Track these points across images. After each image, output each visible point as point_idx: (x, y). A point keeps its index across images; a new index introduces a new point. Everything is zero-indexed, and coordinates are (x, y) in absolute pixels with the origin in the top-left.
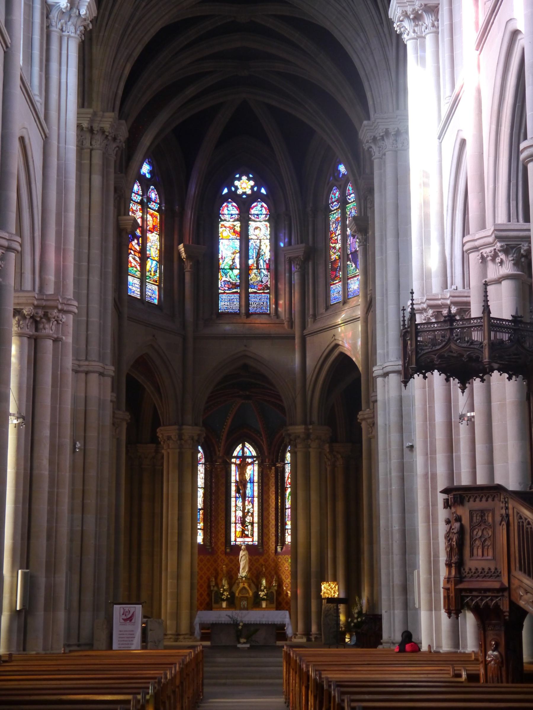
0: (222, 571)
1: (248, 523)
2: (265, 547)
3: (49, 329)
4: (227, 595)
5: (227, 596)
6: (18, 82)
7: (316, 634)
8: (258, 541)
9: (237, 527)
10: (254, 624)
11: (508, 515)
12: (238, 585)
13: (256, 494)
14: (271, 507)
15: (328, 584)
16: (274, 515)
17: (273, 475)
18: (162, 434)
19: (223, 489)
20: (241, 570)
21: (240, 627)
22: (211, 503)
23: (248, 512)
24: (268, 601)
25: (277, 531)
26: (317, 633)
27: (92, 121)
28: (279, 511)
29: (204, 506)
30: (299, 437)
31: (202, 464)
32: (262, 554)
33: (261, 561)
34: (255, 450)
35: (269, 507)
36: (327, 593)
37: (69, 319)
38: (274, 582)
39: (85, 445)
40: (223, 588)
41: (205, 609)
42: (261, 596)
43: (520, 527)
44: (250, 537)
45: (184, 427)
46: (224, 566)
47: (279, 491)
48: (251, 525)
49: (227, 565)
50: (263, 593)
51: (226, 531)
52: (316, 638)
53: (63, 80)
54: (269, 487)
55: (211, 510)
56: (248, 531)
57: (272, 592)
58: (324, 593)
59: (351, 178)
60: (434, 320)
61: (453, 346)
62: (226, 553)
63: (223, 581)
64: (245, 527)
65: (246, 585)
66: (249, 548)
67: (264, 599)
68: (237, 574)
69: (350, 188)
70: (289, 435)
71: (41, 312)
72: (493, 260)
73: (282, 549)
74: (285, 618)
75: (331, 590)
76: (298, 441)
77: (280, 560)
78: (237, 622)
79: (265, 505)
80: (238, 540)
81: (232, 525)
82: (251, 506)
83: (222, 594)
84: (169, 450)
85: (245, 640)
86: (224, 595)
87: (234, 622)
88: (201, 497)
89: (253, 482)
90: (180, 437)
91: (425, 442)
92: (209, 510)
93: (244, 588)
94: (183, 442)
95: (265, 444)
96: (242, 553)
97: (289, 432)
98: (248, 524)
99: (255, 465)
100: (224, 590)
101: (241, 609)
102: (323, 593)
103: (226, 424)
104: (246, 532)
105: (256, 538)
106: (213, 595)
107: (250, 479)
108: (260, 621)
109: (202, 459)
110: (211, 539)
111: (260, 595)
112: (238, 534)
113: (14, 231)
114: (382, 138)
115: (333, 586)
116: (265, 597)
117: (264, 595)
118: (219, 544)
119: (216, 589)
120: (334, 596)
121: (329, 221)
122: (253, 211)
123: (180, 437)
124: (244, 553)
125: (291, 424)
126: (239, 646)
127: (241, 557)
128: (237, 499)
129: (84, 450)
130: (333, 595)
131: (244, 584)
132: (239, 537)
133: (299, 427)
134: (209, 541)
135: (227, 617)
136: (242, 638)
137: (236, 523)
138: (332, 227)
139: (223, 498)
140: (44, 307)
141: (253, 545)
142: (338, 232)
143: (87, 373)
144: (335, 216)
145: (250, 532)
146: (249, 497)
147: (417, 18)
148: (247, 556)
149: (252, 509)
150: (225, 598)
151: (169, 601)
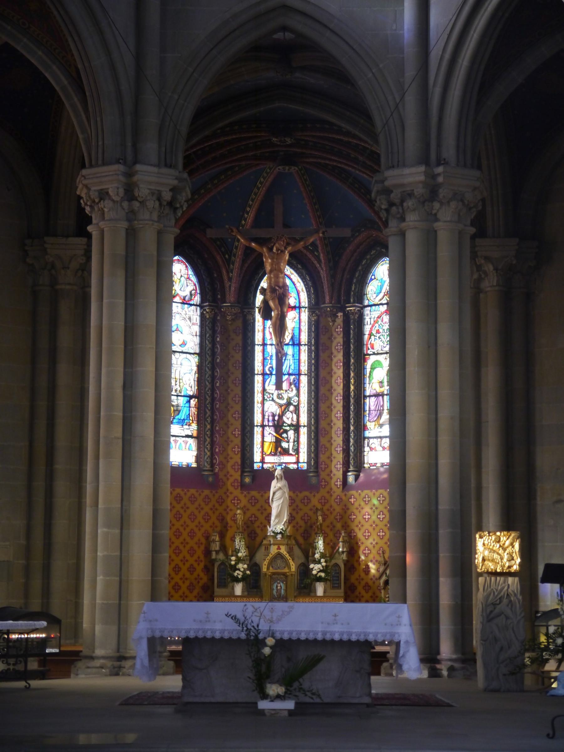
0: (235, 521)
1: (289, 426)
2: (323, 475)
5: (244, 572)
7: (451, 660)
8: (308, 463)
9: (266, 433)
10: (307, 641)
12: (267, 548)
13: (304, 368)
14: (335, 394)
15: (493, 538)
16: (341, 409)
17: (340, 330)
18: (86, 186)
19: (238, 357)
20: (273, 518)
21: (267, 651)
22: (213, 383)
23: (289, 404)
24: (328, 583)
25: (346, 441)
26: (454, 656)
28: (352, 401)
29: (199, 390)
30: (411, 195)
31: (196, 305)
32: (315, 488)
33: (315, 502)
34: (302, 279)
35: (332, 394)
36: (493, 560)
40: (237, 556)
41: (200, 598)
42: (314, 572)
44: (291, 455)
45: (138, 167)
46: (239, 512)
47: (352, 361)
48: (294, 430)
49: (245, 510)
50: (319, 566)
51: (243, 441)
52: (451, 669)
54: (332, 353)
55: (213, 399)
56: (288, 442)
57: (336, 565)
58: (484, 560)
62: (243, 486)
63: (237, 540)
65: (283, 550)
66: (288, 474)
67: (320, 579)
68: (265, 526)
70: (387, 191)
73: (357, 478)
74: (399, 624)
75: (501, 551)
76: (409, 203)
77: (352, 500)
78: (256, 636)
79: (322, 390)
80: (268, 459)
81: (256, 429)
82: (295, 392)
83: (235, 568)
84: (102, 224)
85: (281, 690)
86: (239, 570)
87: (248, 635)
88: (194, 372)
89: (299, 345)
92: (209, 399)
93: (279, 556)
94: (136, 204)
95: (323, 265)
96: (275, 485)
97: (387, 183)
98: (288, 428)
99: (303, 309)
100: (239, 560)
101: (273, 599)
102: (481, 559)
103: (243, 222)
104: (284, 445)
105: (303, 457)
106: (216, 570)
108: (324, 633)
109: (195, 296)
110: (212, 457)
111: (312, 569)
112: (268, 448)
115: (507, 543)
116: (323, 575)
117: (321, 571)
118: (229, 465)
119: (221, 556)
120: (509, 567)
124: (279, 485)
126: (263, 705)
127: (274, 493)
128: (266, 377)
130: (507, 565)
132: (270, 454)
133: (413, 170)
134: (209, 460)
135: (229, 619)
136: (271, 683)
137: (263, 426)
139: (238, 374)
141: (298, 471)
145: (291, 444)
146: (289, 374)
148: (286, 490)
150: (240, 577)
151: (101, 577)
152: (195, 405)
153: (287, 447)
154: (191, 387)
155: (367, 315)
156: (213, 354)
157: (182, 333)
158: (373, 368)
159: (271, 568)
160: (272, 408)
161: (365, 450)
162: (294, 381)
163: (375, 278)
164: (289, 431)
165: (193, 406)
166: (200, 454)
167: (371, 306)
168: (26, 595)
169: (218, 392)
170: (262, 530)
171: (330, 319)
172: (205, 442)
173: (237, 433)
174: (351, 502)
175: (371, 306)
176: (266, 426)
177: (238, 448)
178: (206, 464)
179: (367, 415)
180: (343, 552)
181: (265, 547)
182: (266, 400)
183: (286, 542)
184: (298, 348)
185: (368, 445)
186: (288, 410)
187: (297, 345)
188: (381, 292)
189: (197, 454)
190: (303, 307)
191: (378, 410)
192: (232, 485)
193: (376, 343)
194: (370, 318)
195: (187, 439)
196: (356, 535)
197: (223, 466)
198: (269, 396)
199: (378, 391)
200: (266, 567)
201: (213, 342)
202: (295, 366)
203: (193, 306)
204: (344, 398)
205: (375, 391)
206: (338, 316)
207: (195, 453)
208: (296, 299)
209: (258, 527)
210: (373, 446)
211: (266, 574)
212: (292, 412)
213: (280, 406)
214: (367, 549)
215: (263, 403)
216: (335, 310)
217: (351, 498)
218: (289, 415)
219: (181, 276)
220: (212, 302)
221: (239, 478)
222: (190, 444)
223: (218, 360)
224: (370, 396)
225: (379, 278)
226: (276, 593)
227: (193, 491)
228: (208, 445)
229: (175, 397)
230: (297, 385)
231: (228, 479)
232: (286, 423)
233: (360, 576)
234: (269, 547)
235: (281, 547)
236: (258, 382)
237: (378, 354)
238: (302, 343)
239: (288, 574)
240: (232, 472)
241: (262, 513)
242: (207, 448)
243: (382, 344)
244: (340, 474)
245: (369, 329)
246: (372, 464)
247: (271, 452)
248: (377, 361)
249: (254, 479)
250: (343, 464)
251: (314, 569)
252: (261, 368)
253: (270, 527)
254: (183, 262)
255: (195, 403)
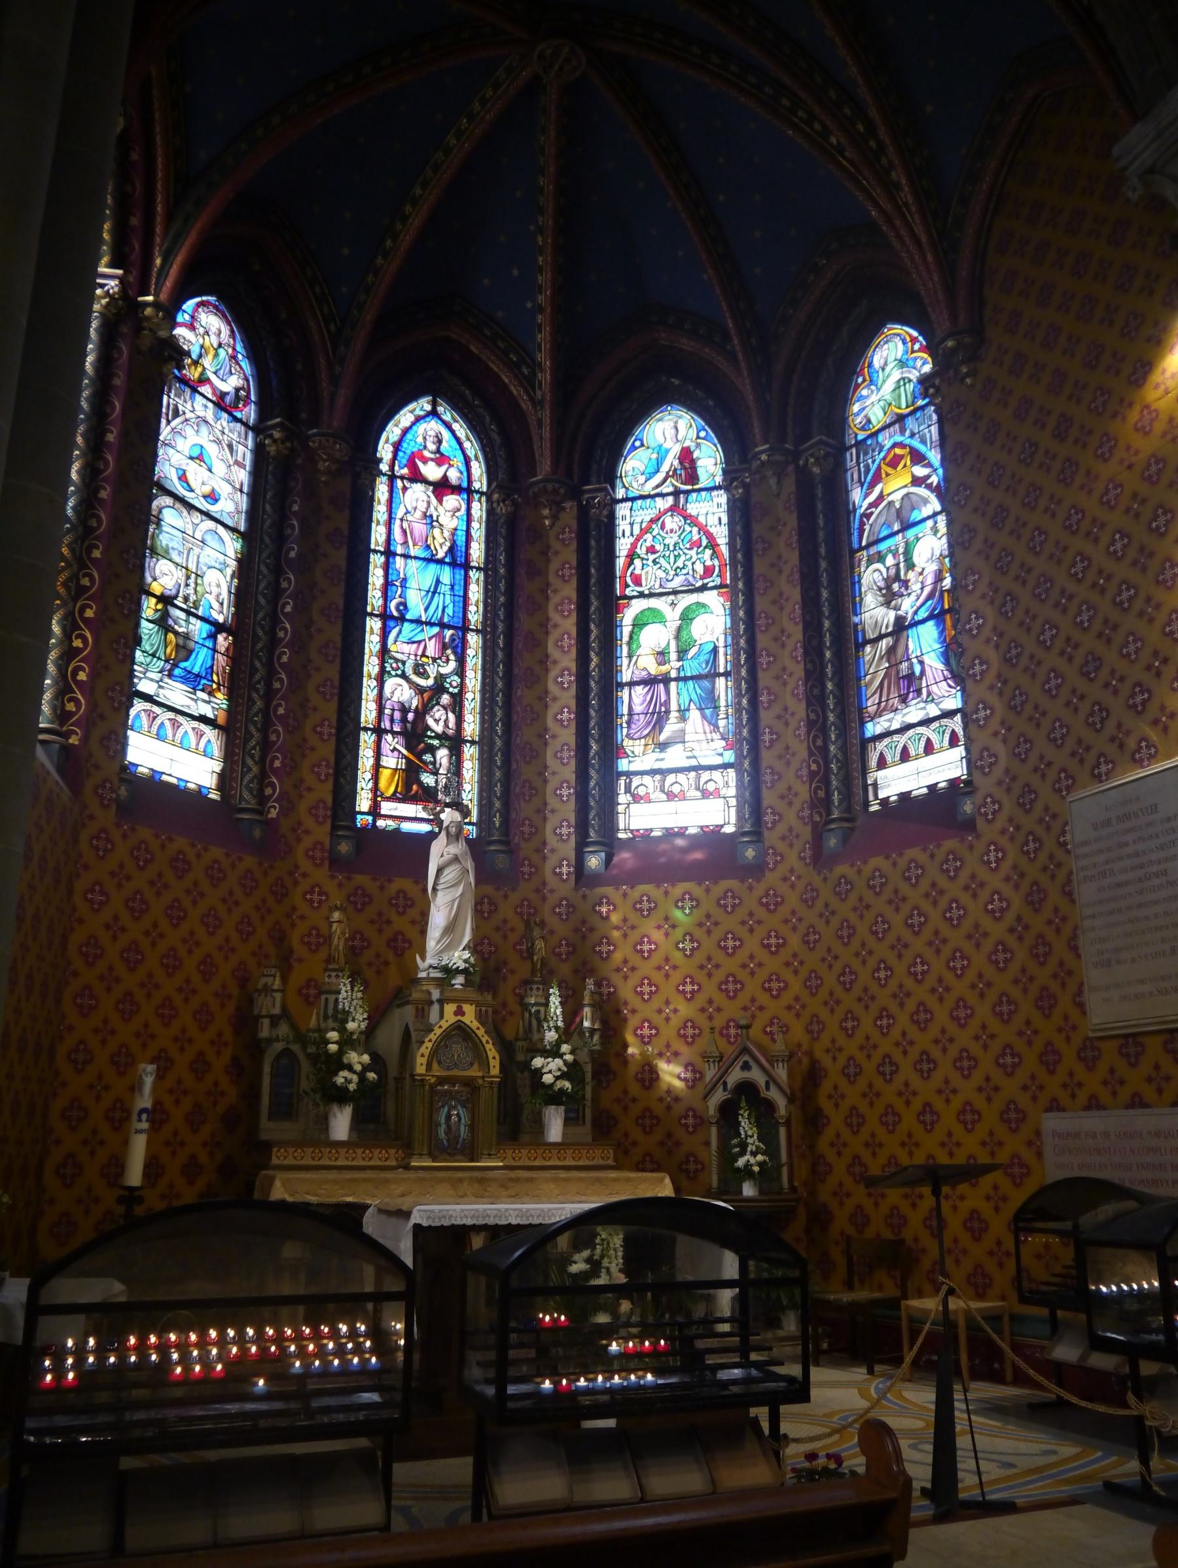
4: (366, 1069)
5: (362, 1076)
9: (386, 748)
13: (475, 616)
23: (439, 687)
35: (547, 670)
38: (587, 1011)
46: (336, 915)
48: (450, 749)
51: (339, 755)
62: (336, 862)
64: (425, 752)
65: (470, 1017)
67: (555, 1097)
80: (386, 808)
82: (452, 665)
83: (337, 1063)
86: (350, 1068)
89: (466, 566)
98: (436, 742)
100: (347, 1042)
103: (389, 243)
104: (428, 779)
106: (267, 1069)
107: (452, 550)
109: (247, 404)
117: (563, 1076)
118: (303, 807)
131: (460, 1012)
132: (393, 798)
149: (456, 680)
150: (352, 1087)
152: (227, 649)
153: (432, 784)
154: (222, 604)
155: (624, 518)
156: (280, 539)
157: (210, 470)
158: (638, 625)
159: (435, 1066)
160: (399, 692)
161: (620, 801)
162: (452, 640)
163: (642, 445)
164: (438, 748)
165: (223, 650)
166: (232, 770)
167: (633, 499)
169: (288, 626)
170: (378, 972)
171: (546, 512)
172: (246, 741)
173: (326, 730)
174: (600, 913)
175: (633, 499)
176: (386, 731)
177: (328, 766)
178: (246, 795)
179: (625, 725)
180: (592, 1031)
181: (417, 1009)
182: (389, 672)
183: (474, 995)
184: (462, 572)
185: (628, 790)
186: (438, 703)
187: (461, 566)
188: (658, 471)
189: (223, 770)
190: (477, 492)
191: (653, 713)
192: (307, 856)
193: (647, 573)
194: (632, 524)
195: (203, 727)
196: (615, 992)
197: (288, 804)
198: (394, 665)
199: (653, 672)
200: (424, 1060)
201: (282, 516)
202: (457, 609)
203: (239, 425)
204: (578, 680)
205: (644, 673)
206: (564, 509)
207: (217, 767)
208: (461, 473)
209: (370, 964)
210: (641, 791)
211: (422, 1080)
212: (445, 708)
213: (420, 690)
214: (646, 1025)
215: (381, 679)
216: (562, 491)
217: (600, 904)
218: (438, 713)
219: (220, 345)
221: (327, 841)
222: (209, 741)
223: (292, 554)
224: (631, 684)
225: (653, 444)
226: (446, 1133)
227: (217, 852)
228: (254, 748)
229: (182, 615)
230: (459, 650)
231: (299, 840)
232: (433, 731)
233: (626, 1092)
234: (426, 1008)
235: (467, 1008)
236: (372, 632)
237: (651, 595)
238: (472, 564)
239: (480, 1081)
240: (309, 823)
241: (380, 931)
242: (252, 756)
243: (663, 575)
245: (629, 546)
246: (638, 830)
247: (395, 792)
248: (649, 608)
249: (359, 847)
250: (577, 827)
251: (544, 1071)
252: (381, 602)
253: (423, 958)
254: (224, 316)
255: (226, 644)
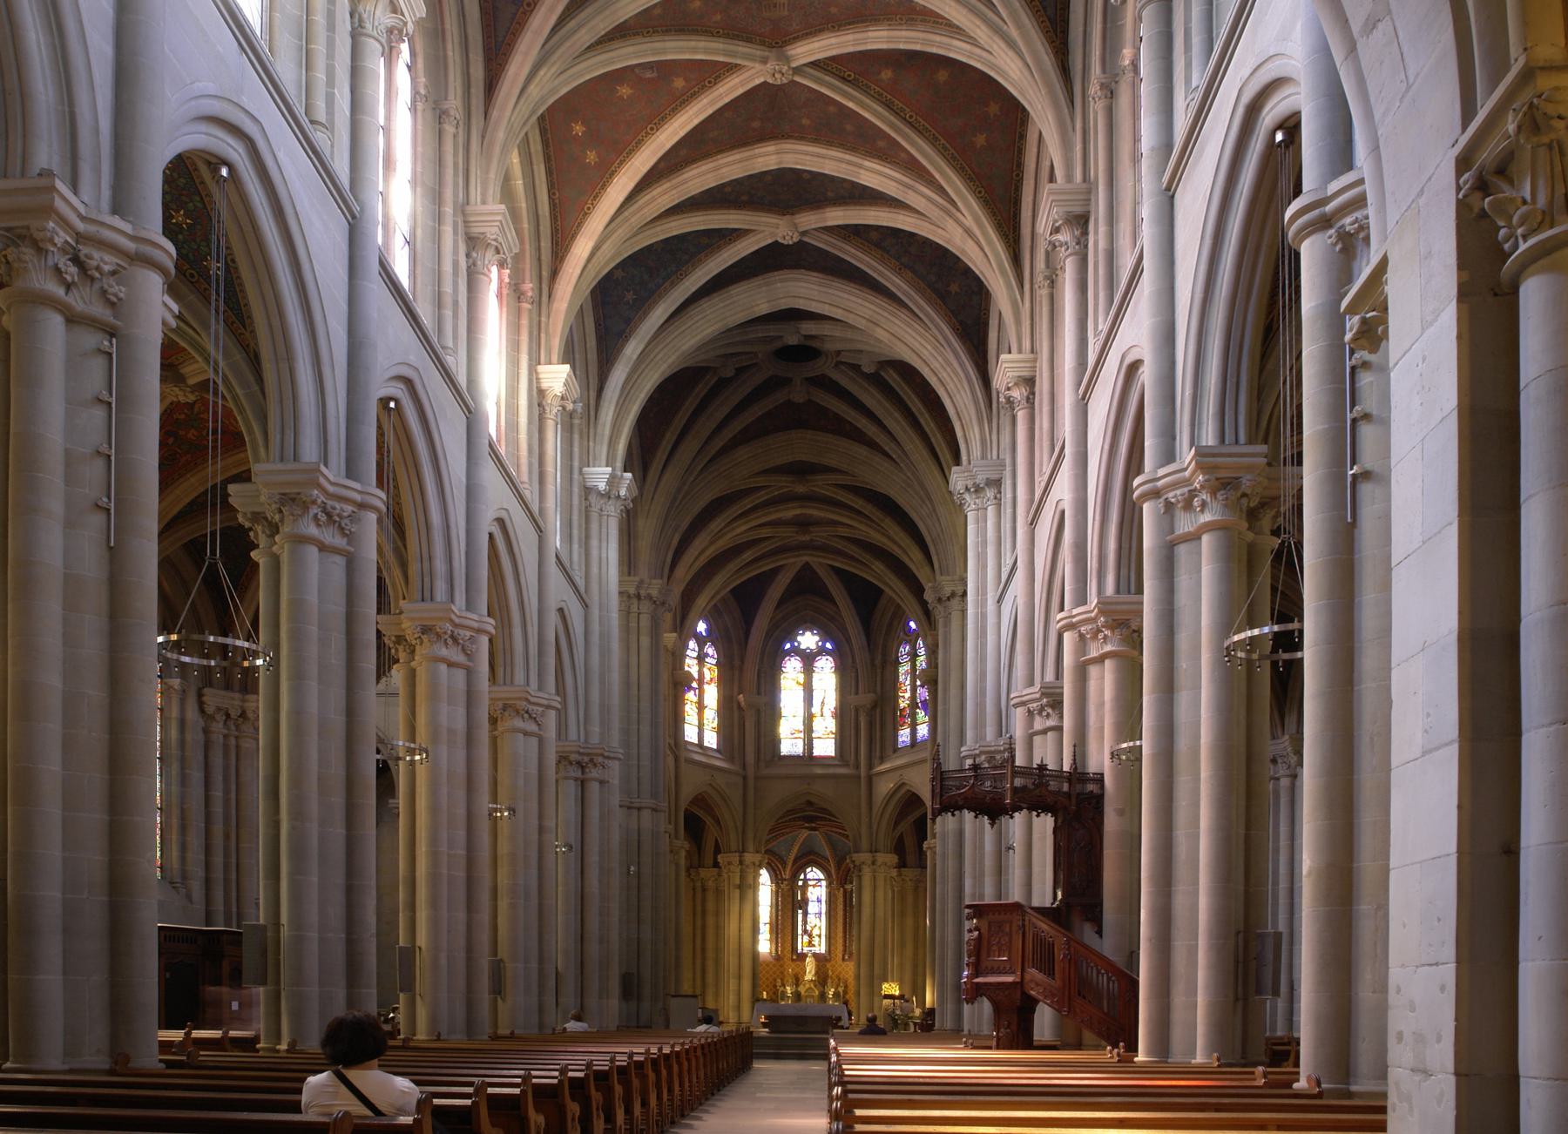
3: (594, 773)
6: (554, 559)
11: (1024, 925)
27: (638, 587)
32: (829, 961)
37: (615, 765)
39: (639, 869)
43: (1036, 935)
45: (746, 854)
53: (604, 555)
59: (921, 633)
60: (987, 765)
61: (976, 790)
62: (793, 960)
66: (815, 955)
69: (920, 642)
71: (586, 759)
72: (1040, 713)
90: (741, 862)
91: (975, 869)
93: (810, 988)
112: (805, 944)
113: (554, 691)
114: (948, 599)
121: (898, 673)
122: (816, 664)
123: (741, 862)
125: (857, 852)
129: (639, 874)
138: (901, 679)
140: (588, 754)
141: (820, 954)
142: (908, 682)
143: (639, 809)
144: (904, 669)
147: (978, 490)
168: (694, 987)
220: (1270, 1066)
244: (841, 956)
